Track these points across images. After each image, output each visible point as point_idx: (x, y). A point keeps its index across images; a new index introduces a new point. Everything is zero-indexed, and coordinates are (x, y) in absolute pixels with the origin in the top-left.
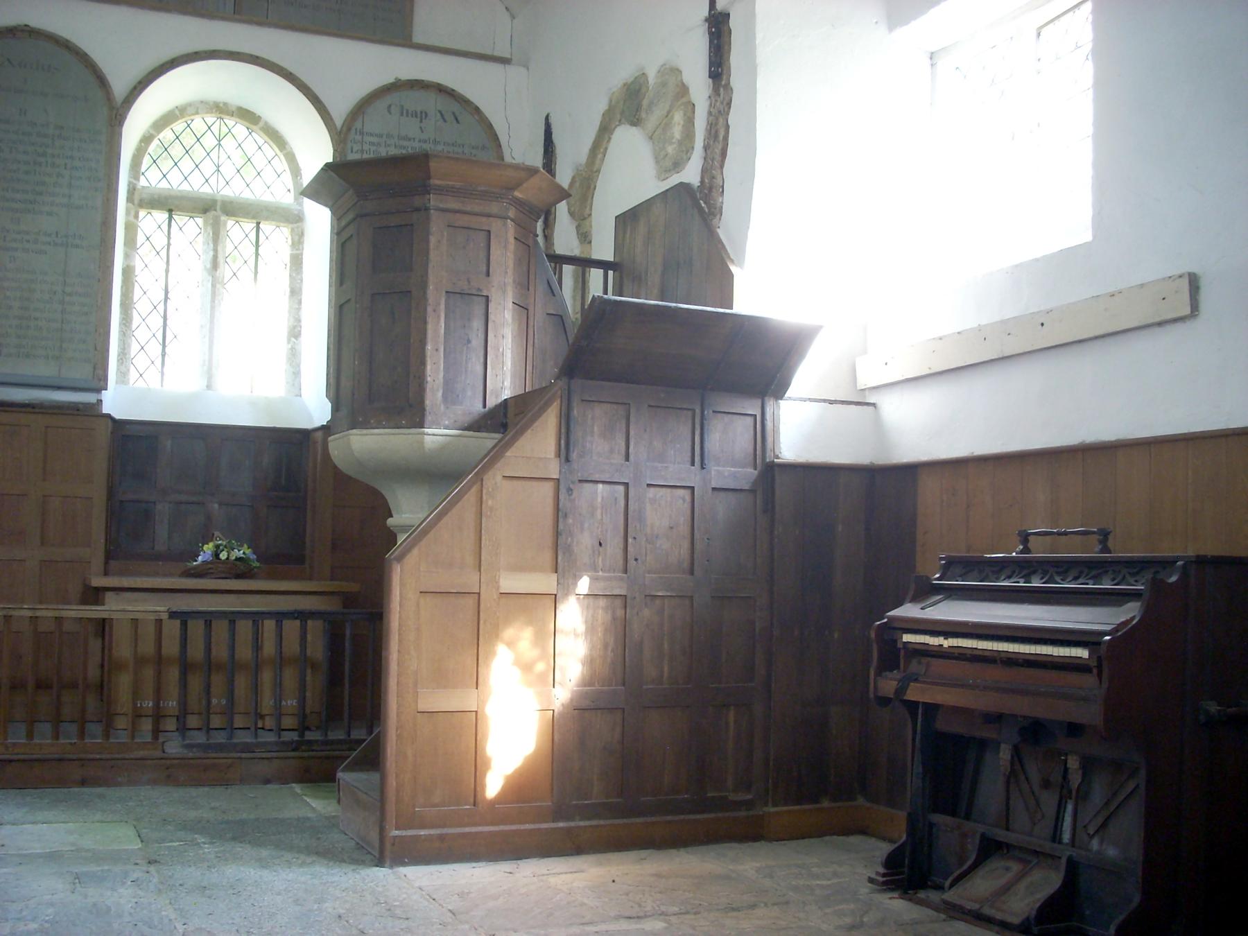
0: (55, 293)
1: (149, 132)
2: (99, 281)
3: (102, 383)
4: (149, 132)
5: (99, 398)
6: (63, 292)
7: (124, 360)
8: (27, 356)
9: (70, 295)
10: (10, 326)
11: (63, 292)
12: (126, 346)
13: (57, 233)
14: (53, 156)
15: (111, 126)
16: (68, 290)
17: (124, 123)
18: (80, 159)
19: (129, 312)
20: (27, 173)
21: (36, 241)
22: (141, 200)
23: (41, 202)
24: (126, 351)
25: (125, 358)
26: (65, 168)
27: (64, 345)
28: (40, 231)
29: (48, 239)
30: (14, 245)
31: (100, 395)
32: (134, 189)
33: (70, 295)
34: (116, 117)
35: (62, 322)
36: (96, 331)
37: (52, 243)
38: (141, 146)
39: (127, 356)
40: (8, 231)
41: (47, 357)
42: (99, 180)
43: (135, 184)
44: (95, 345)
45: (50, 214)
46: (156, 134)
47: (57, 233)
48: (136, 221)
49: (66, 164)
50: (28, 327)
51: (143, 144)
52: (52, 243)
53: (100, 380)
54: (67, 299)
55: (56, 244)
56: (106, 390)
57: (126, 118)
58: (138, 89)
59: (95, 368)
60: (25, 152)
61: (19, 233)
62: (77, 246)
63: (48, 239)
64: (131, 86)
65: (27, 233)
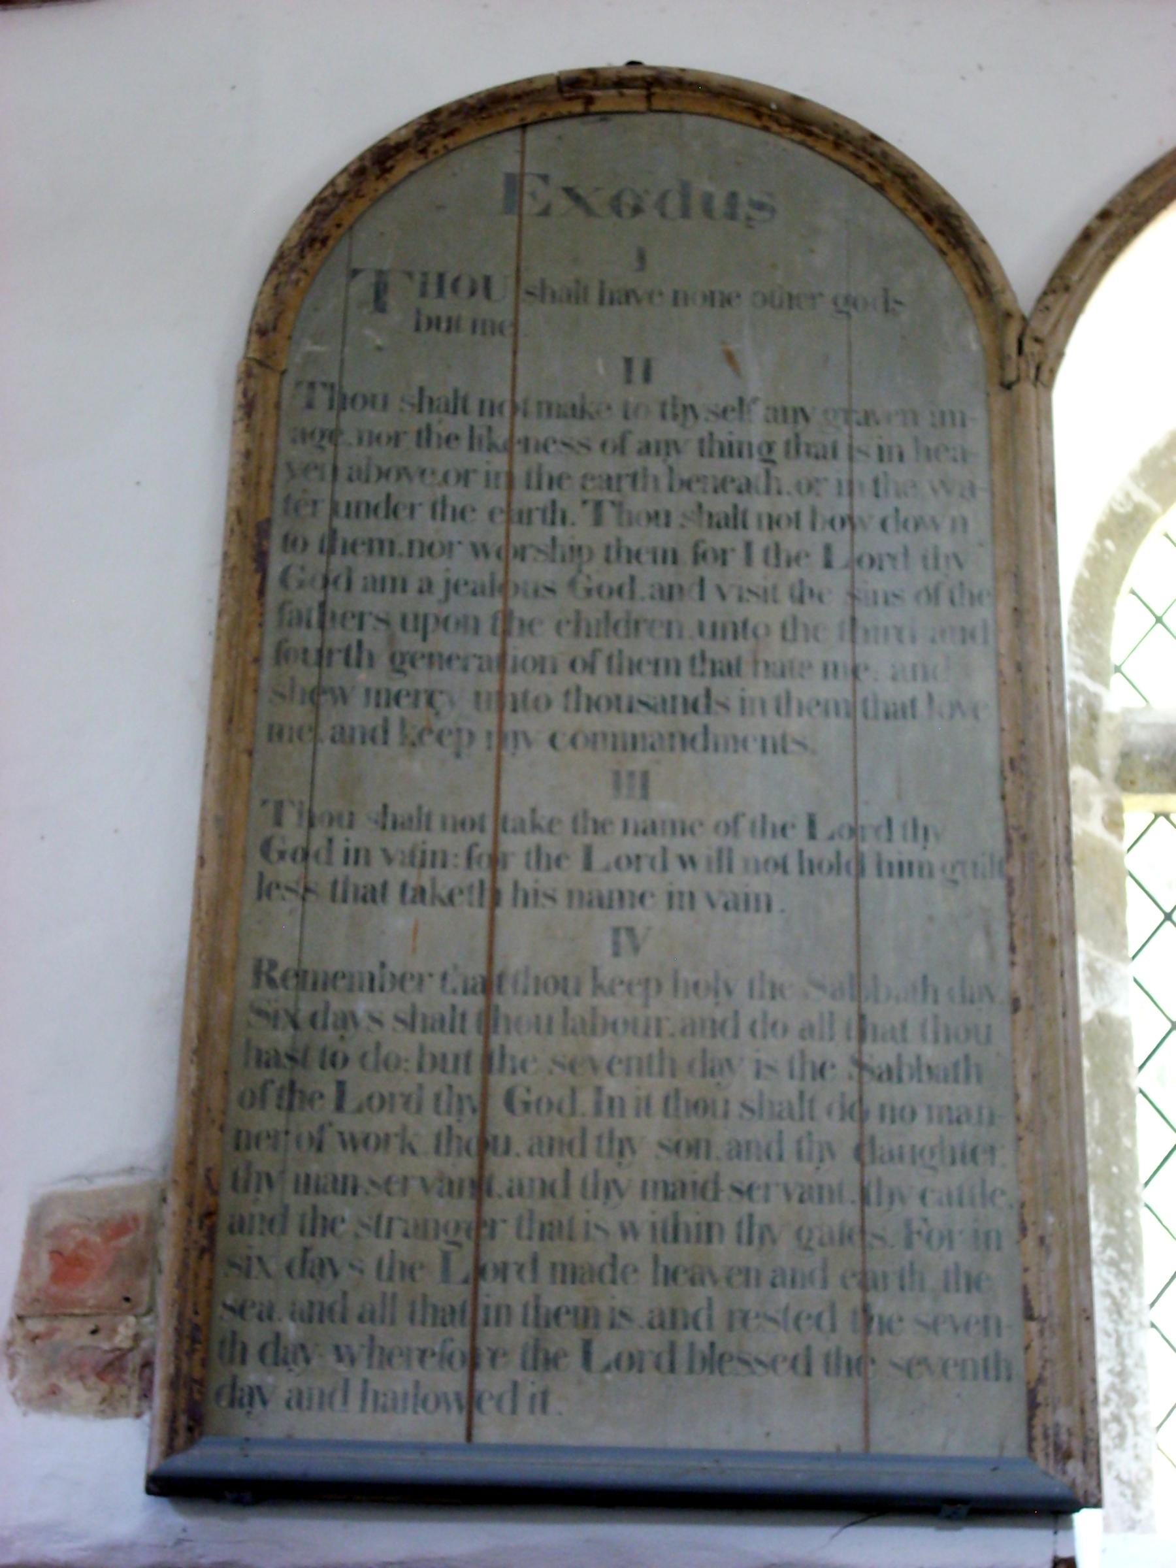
0: (821, 1071)
1: (1128, 496)
2: (1015, 1005)
3: (1074, 1468)
4: (1128, 496)
5: (1064, 1554)
6: (860, 1065)
7: (1128, 1422)
8: (714, 1361)
9: (889, 1074)
10: (629, 1230)
11: (860, 1065)
12: (1130, 1362)
13: (812, 823)
14: (773, 522)
15: (1008, 386)
16: (879, 1053)
17: (1053, 372)
18: (883, 525)
19: (1128, 1213)
20: (668, 593)
21: (723, 861)
22: (1125, 756)
23: (735, 705)
24: (1132, 1385)
25: (1132, 1416)
26: (828, 565)
27: (881, 1304)
28: (736, 820)
29: (775, 848)
30: (628, 880)
31: (1061, 1534)
32: (1094, 717)
33: (889, 1074)
34: (1020, 351)
35: (864, 1198)
36: (1023, 1230)
37: (793, 865)
38: (1105, 550)
39: (1138, 1409)
40: (600, 827)
41: (802, 1364)
42: (975, 599)
43: (1096, 695)
44: (1025, 1290)
45: (777, 746)
46: (1156, 507)
47: (812, 823)
48: (1109, 838)
49: (828, 548)
50: (708, 1232)
51: (1109, 544)
52: (793, 865)
53: (1068, 1456)
54: (878, 1093)
55: (811, 867)
56: (1098, 1504)
57: (1060, 355)
58: (1101, 240)
59: (1033, 1405)
60: (653, 517)
61: (650, 829)
62: (903, 869)
63: (775, 848)
64: (1072, 233)
65: (684, 829)
